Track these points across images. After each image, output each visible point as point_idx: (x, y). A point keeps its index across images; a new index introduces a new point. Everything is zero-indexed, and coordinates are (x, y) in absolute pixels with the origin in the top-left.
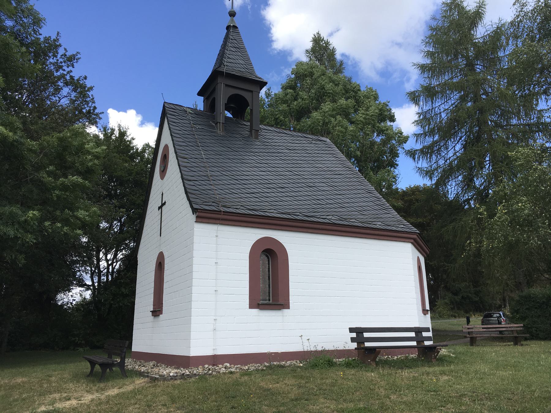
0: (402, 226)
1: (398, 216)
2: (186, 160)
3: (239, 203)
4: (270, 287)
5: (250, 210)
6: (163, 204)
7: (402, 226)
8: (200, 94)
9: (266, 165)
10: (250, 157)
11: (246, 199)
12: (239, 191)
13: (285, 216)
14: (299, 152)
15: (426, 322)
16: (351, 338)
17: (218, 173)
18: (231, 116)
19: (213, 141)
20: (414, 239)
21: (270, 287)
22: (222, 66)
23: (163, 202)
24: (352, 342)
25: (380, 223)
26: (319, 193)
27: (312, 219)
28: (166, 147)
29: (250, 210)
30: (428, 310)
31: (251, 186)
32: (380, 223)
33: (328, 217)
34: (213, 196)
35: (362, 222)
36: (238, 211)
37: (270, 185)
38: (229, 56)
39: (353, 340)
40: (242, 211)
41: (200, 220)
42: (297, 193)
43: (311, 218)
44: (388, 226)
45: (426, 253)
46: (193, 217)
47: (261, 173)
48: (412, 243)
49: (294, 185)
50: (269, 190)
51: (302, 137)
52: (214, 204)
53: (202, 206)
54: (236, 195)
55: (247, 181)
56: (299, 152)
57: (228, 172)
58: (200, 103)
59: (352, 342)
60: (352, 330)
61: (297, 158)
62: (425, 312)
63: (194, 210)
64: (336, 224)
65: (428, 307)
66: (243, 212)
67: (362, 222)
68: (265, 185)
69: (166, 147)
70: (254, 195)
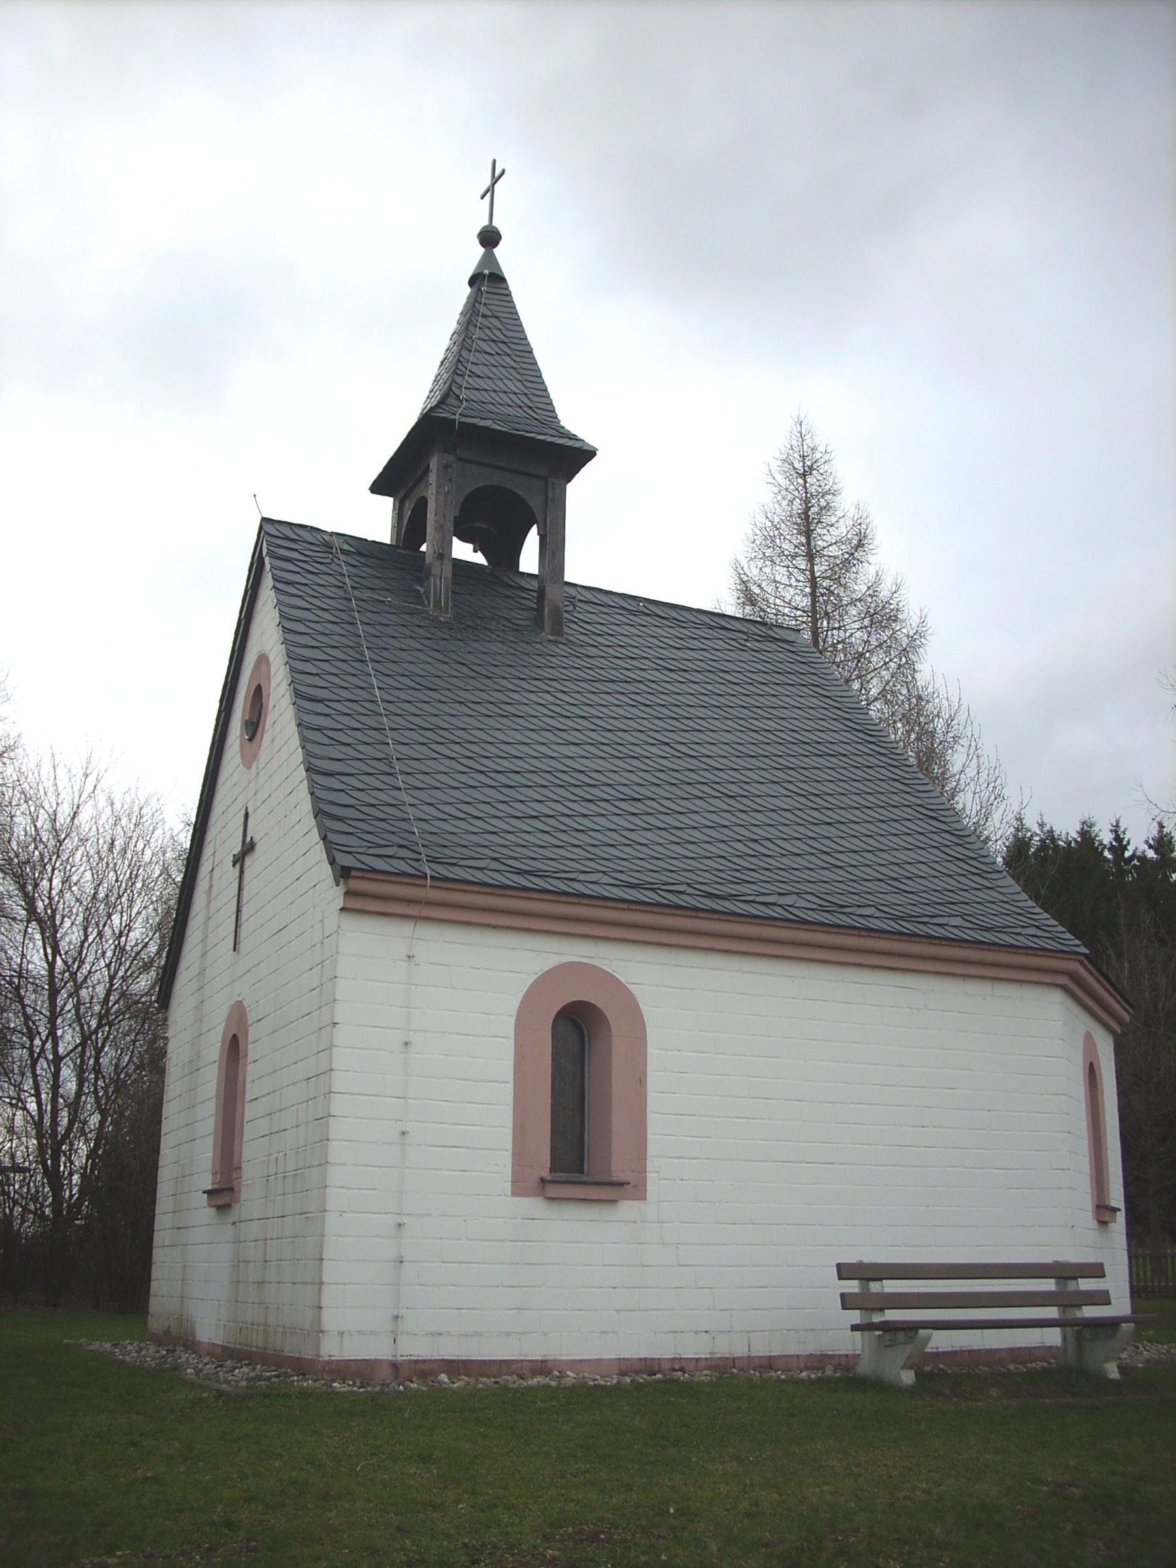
0: (1033, 931)
1: (1024, 896)
2: (320, 708)
3: (486, 851)
4: (577, 1118)
5: (521, 872)
6: (248, 848)
7: (1033, 931)
8: (379, 487)
9: (585, 723)
10: (533, 697)
11: (511, 837)
12: (487, 808)
13: (636, 895)
14: (697, 677)
15: (1113, 1251)
16: (842, 1295)
17: (423, 749)
18: (480, 559)
19: (412, 643)
20: (1073, 976)
21: (577, 1118)
22: (451, 400)
23: (497, 173)
24: (1101, 1265)
25: (958, 921)
26: (760, 816)
27: (728, 905)
28: (263, 659)
29: (521, 872)
30: (1115, 1210)
31: (530, 792)
32: (958, 921)
33: (783, 901)
34: (403, 825)
35: (895, 918)
36: (481, 876)
37: (593, 791)
38: (474, 369)
39: (847, 1302)
40: (497, 876)
41: (358, 904)
42: (682, 818)
43: (727, 904)
44: (987, 929)
45: (1120, 1021)
46: (334, 896)
47: (566, 750)
48: (1064, 988)
49: (674, 789)
50: (591, 806)
51: (711, 628)
52: (403, 853)
53: (362, 858)
54: (480, 823)
55: (517, 777)
56: (697, 677)
57: (457, 748)
58: (375, 520)
59: (1101, 1265)
60: (844, 1271)
61: (692, 700)
62: (1103, 1212)
63: (343, 874)
64: (806, 922)
65: (1116, 1196)
66: (501, 879)
67: (895, 918)
68: (578, 791)
69: (263, 659)
70: (536, 823)
